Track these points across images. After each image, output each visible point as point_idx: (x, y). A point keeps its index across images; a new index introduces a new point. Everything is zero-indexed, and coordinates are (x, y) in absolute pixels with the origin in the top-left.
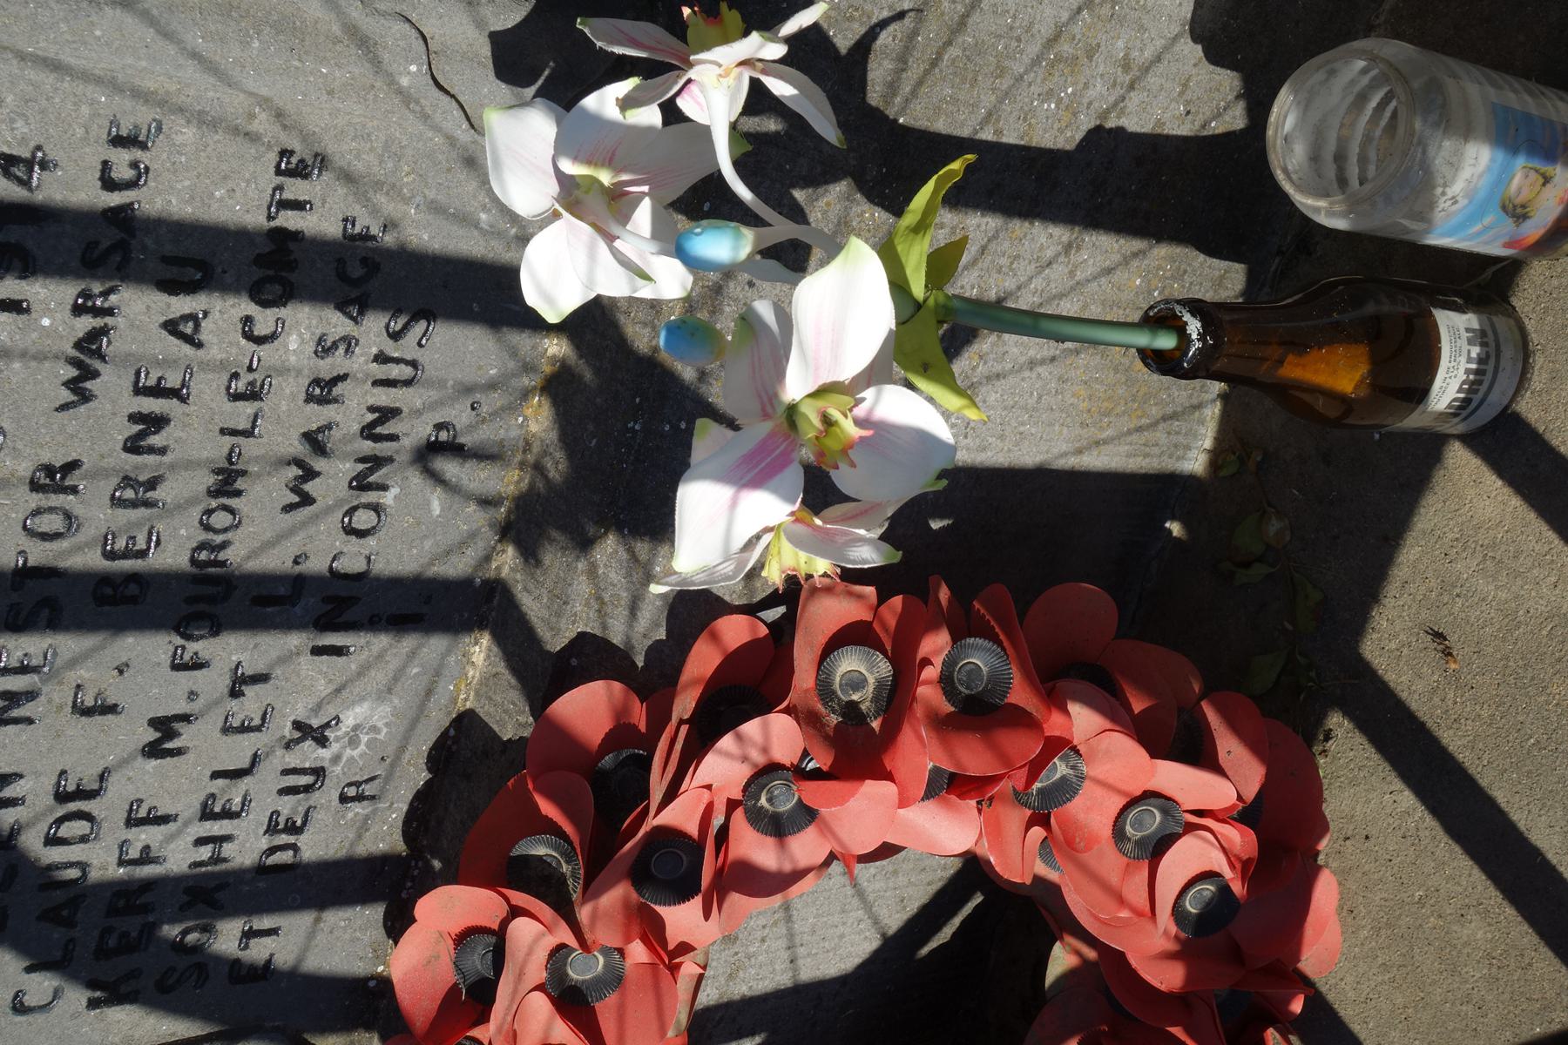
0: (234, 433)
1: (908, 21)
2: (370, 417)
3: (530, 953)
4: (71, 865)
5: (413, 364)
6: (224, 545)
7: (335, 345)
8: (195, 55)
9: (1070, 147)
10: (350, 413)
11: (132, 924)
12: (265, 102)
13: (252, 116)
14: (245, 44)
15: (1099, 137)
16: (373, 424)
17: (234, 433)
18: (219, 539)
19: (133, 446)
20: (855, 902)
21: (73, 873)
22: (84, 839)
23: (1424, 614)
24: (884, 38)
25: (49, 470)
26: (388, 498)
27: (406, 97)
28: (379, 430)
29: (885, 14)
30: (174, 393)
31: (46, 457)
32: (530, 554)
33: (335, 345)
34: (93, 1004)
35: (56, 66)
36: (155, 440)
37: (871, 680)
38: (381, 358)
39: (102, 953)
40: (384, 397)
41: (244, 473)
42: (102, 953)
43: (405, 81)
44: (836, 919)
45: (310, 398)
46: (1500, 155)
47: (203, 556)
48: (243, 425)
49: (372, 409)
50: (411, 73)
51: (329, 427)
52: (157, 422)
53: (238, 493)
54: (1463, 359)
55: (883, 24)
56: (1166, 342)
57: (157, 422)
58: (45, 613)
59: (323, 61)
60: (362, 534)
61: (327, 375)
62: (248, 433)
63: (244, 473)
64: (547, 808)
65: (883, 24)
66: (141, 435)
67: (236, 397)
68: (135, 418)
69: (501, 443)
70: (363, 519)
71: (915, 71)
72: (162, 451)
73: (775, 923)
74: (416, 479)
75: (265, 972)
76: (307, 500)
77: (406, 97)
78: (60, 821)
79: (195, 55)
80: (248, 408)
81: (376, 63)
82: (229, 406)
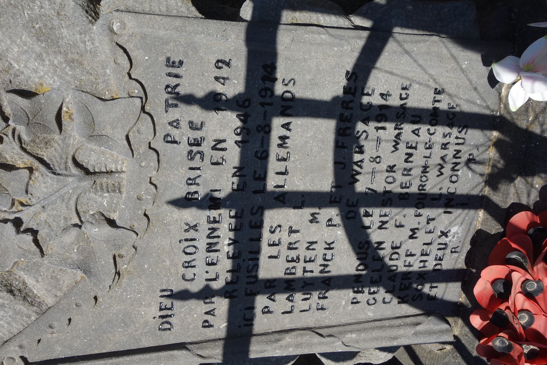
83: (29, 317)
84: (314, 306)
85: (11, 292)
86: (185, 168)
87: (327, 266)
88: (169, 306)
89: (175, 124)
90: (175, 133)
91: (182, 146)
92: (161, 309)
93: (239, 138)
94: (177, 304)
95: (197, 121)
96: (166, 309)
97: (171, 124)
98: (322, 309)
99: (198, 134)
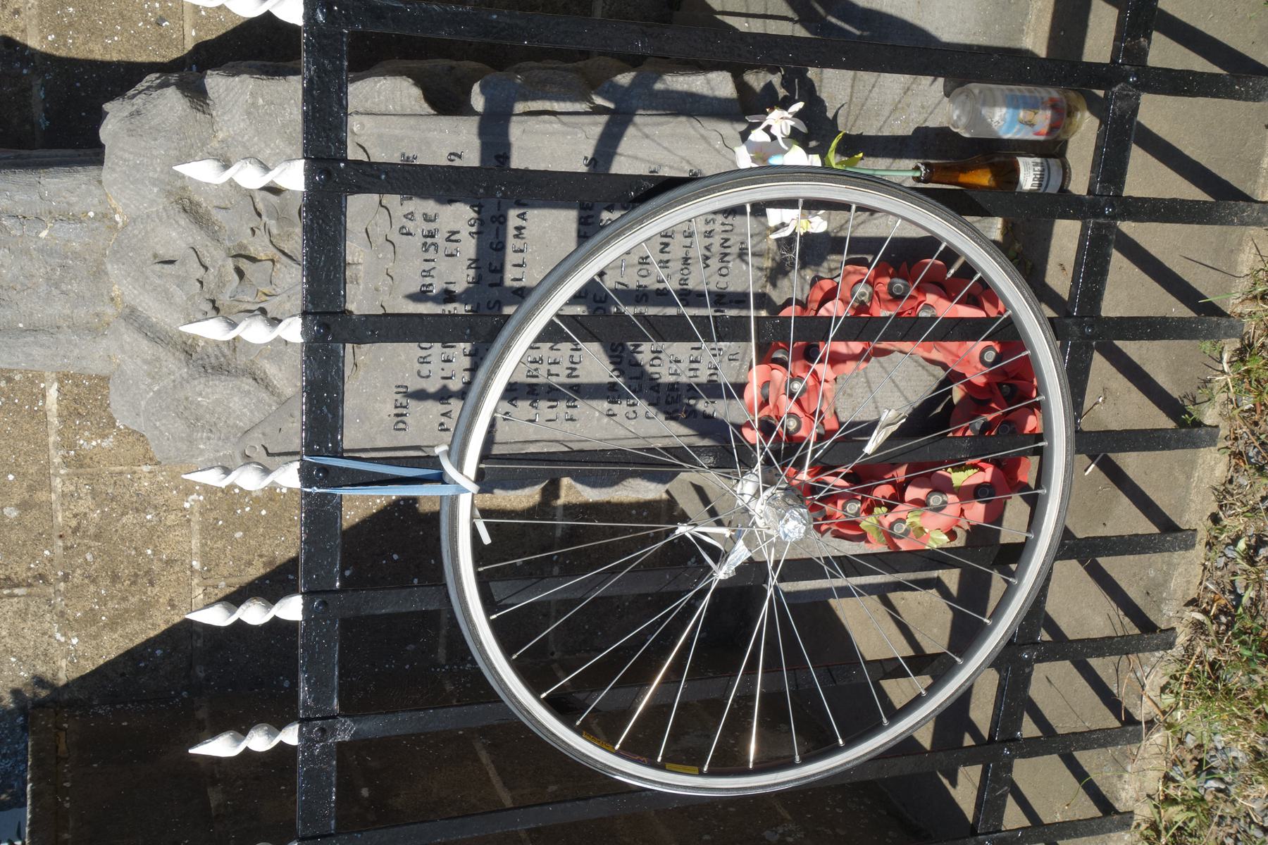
0: (686, 247)
1: (845, 106)
2: (722, 241)
3: (781, 385)
4: (657, 373)
5: (732, 225)
6: (687, 279)
7: (710, 221)
8: (665, 148)
9: (910, 134)
10: (716, 241)
11: (674, 394)
12: (683, 158)
13: (196, 553)
14: (678, 143)
15: (918, 130)
16: (723, 243)
17: (686, 247)
18: (686, 277)
19: (662, 251)
20: (896, 389)
21: (657, 376)
22: (659, 365)
23: (1058, 260)
24: (840, 112)
25: (643, 259)
26: (730, 265)
27: (718, 151)
28: (725, 245)
29: (839, 106)
30: (670, 236)
31: (641, 255)
32: (774, 285)
33: (710, 221)
34: (666, 419)
35: (636, 158)
36: (667, 249)
37: (868, 293)
38: (723, 224)
39: (667, 403)
40: (725, 236)
41: (690, 258)
42: (667, 403)
43: (717, 146)
44: (890, 394)
45: (705, 236)
46: (1011, 110)
47: (682, 282)
48: (689, 245)
49: (722, 239)
50: (719, 144)
51: (711, 244)
52: (667, 245)
53: (689, 264)
54: (1032, 173)
55: (839, 109)
56: (918, 174)
57: (667, 245)
58: (644, 299)
59: (696, 144)
60: (724, 276)
61: (709, 230)
62: (690, 247)
63: (690, 258)
64: (780, 344)
65: (839, 109)
66: (664, 248)
67: (686, 237)
68: (662, 244)
69: (761, 251)
70: (724, 271)
71: (852, 118)
72: (669, 253)
73: (866, 392)
74: (738, 261)
75: (710, 417)
76: (708, 266)
77: (718, 151)
78: (653, 359)
79: (665, 148)
80: (689, 240)
81: (709, 144)
82: (684, 239)
83: (270, 406)
84: (562, 415)
85: (255, 379)
86: (420, 260)
87: (574, 369)
88: (404, 404)
89: (410, 216)
90: (410, 226)
91: (416, 238)
92: (396, 407)
93: (474, 229)
94: (412, 403)
95: (431, 213)
96: (401, 406)
97: (405, 216)
98: (572, 420)
99: (432, 226)
